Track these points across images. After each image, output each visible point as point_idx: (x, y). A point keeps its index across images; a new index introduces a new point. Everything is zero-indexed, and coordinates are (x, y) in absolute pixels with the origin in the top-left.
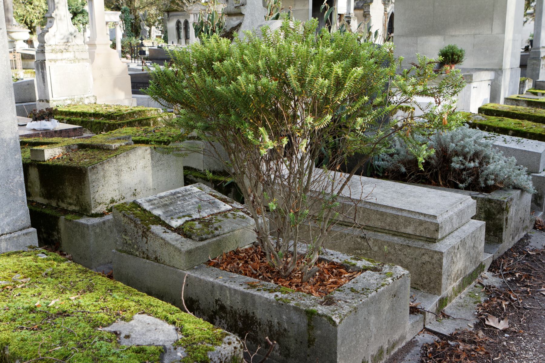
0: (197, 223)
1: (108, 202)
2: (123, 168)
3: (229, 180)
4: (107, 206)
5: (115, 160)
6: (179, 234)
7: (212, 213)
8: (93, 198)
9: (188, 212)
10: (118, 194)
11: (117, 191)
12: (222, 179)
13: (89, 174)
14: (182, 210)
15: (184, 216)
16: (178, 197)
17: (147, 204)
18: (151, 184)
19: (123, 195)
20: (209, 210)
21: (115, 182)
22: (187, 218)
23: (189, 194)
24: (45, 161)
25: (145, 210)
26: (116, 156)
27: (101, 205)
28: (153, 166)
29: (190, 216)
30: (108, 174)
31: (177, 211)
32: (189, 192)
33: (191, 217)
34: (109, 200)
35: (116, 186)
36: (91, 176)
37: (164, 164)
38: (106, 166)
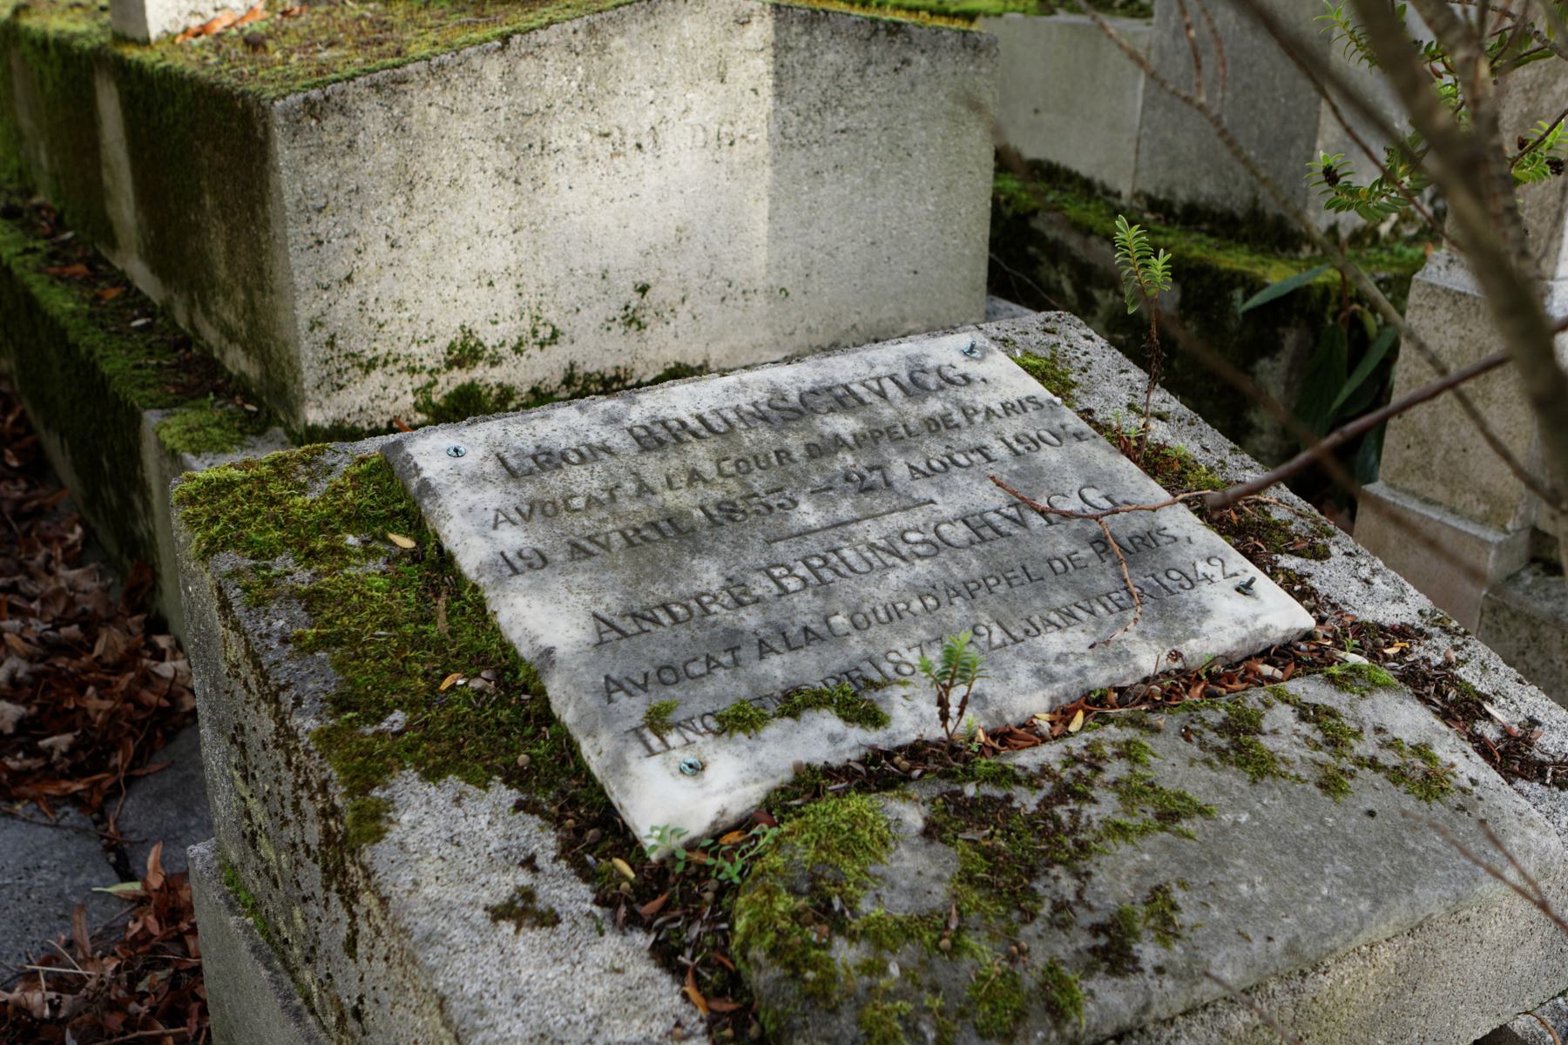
0: (913, 817)
1: (431, 355)
2: (557, 133)
3: (1279, 276)
4: (421, 380)
5: (493, 69)
6: (665, 956)
7: (1099, 678)
8: (315, 324)
9: (856, 646)
10: (509, 309)
11: (506, 289)
12: (1235, 260)
13: (285, 153)
14: (805, 608)
15: (795, 703)
16: (821, 450)
17: (493, 497)
18: (761, 257)
19: (551, 315)
20: (1076, 639)
21: (486, 223)
22: (823, 739)
23: (937, 425)
24: (146, 42)
25: (445, 561)
26: (506, 39)
27: (377, 376)
28: (784, 141)
29: (856, 701)
30: (440, 163)
31: (750, 619)
32: (934, 406)
33: (874, 718)
34: (441, 344)
35: (498, 255)
36: (296, 170)
37: (860, 133)
38: (425, 104)
